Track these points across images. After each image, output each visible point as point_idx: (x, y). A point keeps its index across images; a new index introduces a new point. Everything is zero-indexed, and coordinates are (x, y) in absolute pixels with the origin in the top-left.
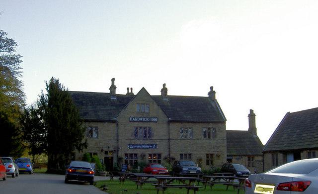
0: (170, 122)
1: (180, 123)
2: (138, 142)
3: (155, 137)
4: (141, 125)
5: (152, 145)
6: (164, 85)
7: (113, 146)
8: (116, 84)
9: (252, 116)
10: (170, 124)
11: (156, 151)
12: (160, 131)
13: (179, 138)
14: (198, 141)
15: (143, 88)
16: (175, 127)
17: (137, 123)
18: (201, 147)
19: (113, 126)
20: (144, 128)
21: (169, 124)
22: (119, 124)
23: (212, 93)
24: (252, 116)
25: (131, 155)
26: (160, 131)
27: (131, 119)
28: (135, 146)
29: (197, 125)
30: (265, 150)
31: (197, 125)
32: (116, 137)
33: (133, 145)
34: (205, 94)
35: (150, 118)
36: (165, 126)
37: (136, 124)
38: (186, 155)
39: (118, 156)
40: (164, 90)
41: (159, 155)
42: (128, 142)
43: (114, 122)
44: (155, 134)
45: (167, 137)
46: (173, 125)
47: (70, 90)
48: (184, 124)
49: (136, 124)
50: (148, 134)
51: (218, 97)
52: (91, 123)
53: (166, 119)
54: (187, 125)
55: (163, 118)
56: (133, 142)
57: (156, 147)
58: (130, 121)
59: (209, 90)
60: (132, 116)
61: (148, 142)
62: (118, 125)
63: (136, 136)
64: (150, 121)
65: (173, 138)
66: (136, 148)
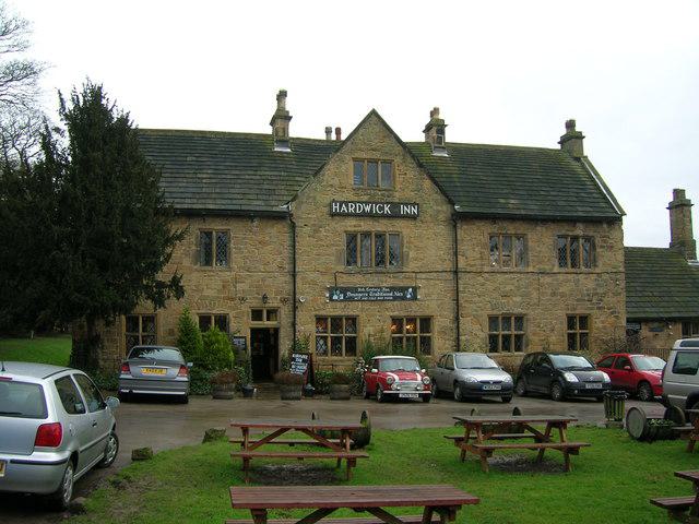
0: (457, 219)
2: (356, 281)
3: (412, 266)
6: (282, 95)
8: (289, 105)
11: (415, 310)
16: (474, 238)
23: (572, 137)
32: (288, 267)
33: (344, 291)
34: (550, 140)
35: (395, 206)
36: (443, 230)
37: (351, 225)
44: (412, 254)
49: (351, 225)
50: (386, 255)
51: (590, 149)
53: (445, 209)
54: (511, 228)
55: (436, 206)
56: (344, 281)
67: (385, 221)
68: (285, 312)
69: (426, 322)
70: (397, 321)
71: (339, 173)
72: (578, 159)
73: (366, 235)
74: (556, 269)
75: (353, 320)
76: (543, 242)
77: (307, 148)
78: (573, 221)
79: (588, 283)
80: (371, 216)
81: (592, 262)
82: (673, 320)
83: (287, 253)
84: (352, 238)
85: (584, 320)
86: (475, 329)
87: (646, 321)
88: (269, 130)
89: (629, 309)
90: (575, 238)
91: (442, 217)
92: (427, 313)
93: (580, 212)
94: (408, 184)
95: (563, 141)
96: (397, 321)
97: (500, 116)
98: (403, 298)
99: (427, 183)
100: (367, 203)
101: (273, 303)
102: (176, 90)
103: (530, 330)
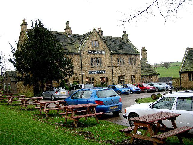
0: (112, 54)
2: (93, 69)
3: (104, 65)
5: (103, 71)
6: (67, 23)
8: (70, 25)
10: (113, 56)
11: (105, 75)
16: (115, 58)
20: (97, 59)
23: (125, 35)
25: (90, 78)
30: (182, 71)
32: (80, 66)
33: (92, 71)
34: (119, 35)
35: (100, 51)
36: (109, 57)
37: (92, 56)
38: (121, 77)
40: (68, 28)
42: (88, 70)
44: (104, 63)
47: (52, 30)
49: (92, 56)
50: (99, 62)
51: (129, 38)
53: (109, 52)
54: (121, 56)
55: (108, 52)
56: (92, 69)
59: (65, 26)
60: (89, 50)
63: (92, 65)
64: (101, 54)
67: (98, 55)
68: (80, 77)
69: (107, 78)
70: (101, 78)
71: (89, 44)
72: (127, 40)
73: (95, 58)
74: (129, 65)
75: (93, 78)
76: (126, 59)
77: (77, 37)
78: (132, 55)
79: (135, 68)
80: (96, 54)
81: (135, 63)
82: (148, 76)
83: (80, 63)
84: (92, 59)
85: (134, 76)
86: (116, 80)
87: (144, 76)
88: (64, 31)
89: (143, 71)
90: (132, 59)
91: (109, 54)
92: (107, 76)
93: (132, 53)
94: (103, 47)
95: (123, 36)
96: (101, 78)
97: (113, 31)
98: (103, 73)
99: (106, 46)
100: (95, 51)
101: (78, 75)
102: (168, 61)
103: (125, 78)
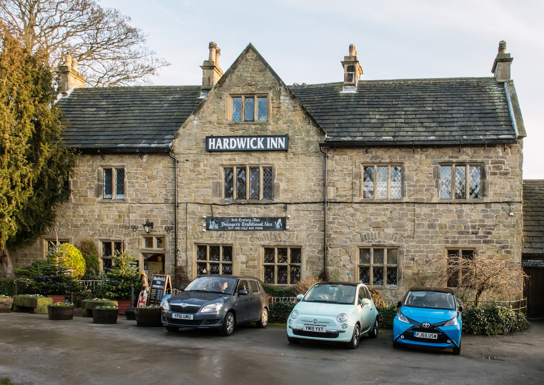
0: (330, 147)
1: (362, 151)
3: (281, 197)
4: (239, 159)
7: (164, 222)
9: (503, 59)
11: (285, 239)
12: (297, 175)
13: (356, 199)
14: (419, 209)
15: (250, 48)
17: (229, 156)
18: (431, 226)
19: (161, 165)
21: (326, 156)
22: (181, 158)
24: (503, 59)
26: (297, 175)
27: (212, 144)
28: (223, 224)
29: (417, 156)
31: (419, 156)
33: (218, 221)
34: (482, 69)
36: (314, 162)
37: (225, 159)
39: (175, 265)
41: (297, 252)
42: (204, 212)
43: (166, 152)
45: (319, 207)
46: (337, 157)
48: (374, 152)
52: (107, 157)
53: (315, 138)
55: (306, 134)
56: (219, 212)
57: (284, 227)
58: (211, 151)
61: (260, 212)
62: (175, 161)
65: (339, 199)
66: (225, 229)
